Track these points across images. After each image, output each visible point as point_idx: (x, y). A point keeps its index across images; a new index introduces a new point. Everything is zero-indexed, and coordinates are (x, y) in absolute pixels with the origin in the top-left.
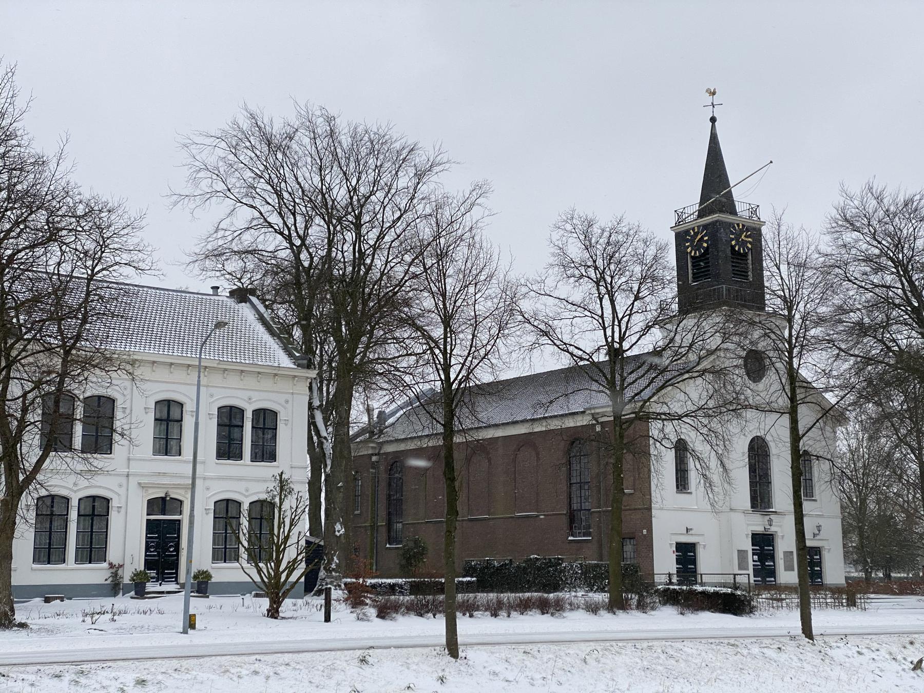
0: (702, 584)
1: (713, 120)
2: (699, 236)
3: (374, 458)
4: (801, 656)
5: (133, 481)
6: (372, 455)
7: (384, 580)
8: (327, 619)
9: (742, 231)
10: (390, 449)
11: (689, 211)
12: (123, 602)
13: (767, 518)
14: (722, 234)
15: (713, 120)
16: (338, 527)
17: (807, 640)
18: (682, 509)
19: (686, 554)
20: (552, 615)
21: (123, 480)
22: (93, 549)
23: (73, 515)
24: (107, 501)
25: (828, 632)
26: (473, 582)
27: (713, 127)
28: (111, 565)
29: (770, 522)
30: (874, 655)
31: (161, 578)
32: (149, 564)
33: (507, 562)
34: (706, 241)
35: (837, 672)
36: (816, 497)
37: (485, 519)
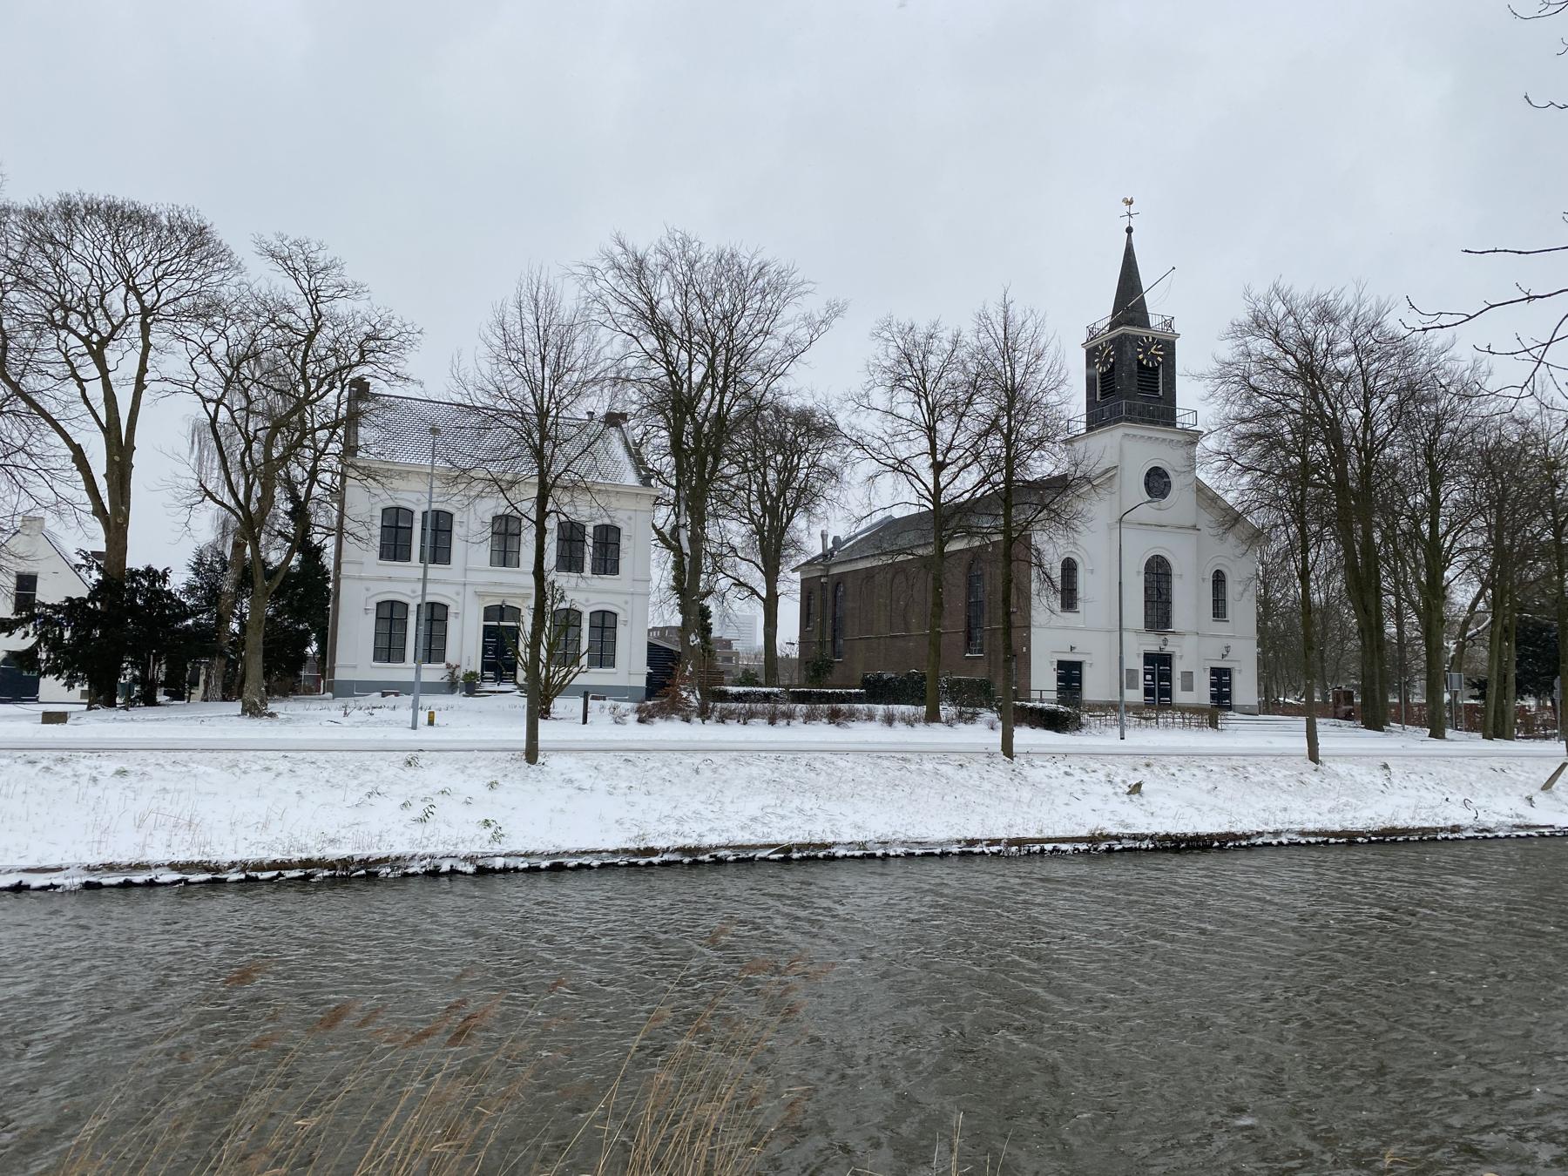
1: (1129, 230)
4: (985, 775)
5: (470, 589)
8: (585, 722)
9: (1152, 344)
10: (835, 571)
12: (457, 699)
15: (1129, 230)
16: (692, 637)
19: (1070, 674)
21: (461, 589)
22: (433, 649)
23: (585, 626)
24: (446, 607)
25: (1036, 750)
27: (1129, 237)
28: (449, 666)
29: (1165, 642)
30: (1085, 777)
31: (500, 678)
32: (486, 666)
35: (1026, 794)
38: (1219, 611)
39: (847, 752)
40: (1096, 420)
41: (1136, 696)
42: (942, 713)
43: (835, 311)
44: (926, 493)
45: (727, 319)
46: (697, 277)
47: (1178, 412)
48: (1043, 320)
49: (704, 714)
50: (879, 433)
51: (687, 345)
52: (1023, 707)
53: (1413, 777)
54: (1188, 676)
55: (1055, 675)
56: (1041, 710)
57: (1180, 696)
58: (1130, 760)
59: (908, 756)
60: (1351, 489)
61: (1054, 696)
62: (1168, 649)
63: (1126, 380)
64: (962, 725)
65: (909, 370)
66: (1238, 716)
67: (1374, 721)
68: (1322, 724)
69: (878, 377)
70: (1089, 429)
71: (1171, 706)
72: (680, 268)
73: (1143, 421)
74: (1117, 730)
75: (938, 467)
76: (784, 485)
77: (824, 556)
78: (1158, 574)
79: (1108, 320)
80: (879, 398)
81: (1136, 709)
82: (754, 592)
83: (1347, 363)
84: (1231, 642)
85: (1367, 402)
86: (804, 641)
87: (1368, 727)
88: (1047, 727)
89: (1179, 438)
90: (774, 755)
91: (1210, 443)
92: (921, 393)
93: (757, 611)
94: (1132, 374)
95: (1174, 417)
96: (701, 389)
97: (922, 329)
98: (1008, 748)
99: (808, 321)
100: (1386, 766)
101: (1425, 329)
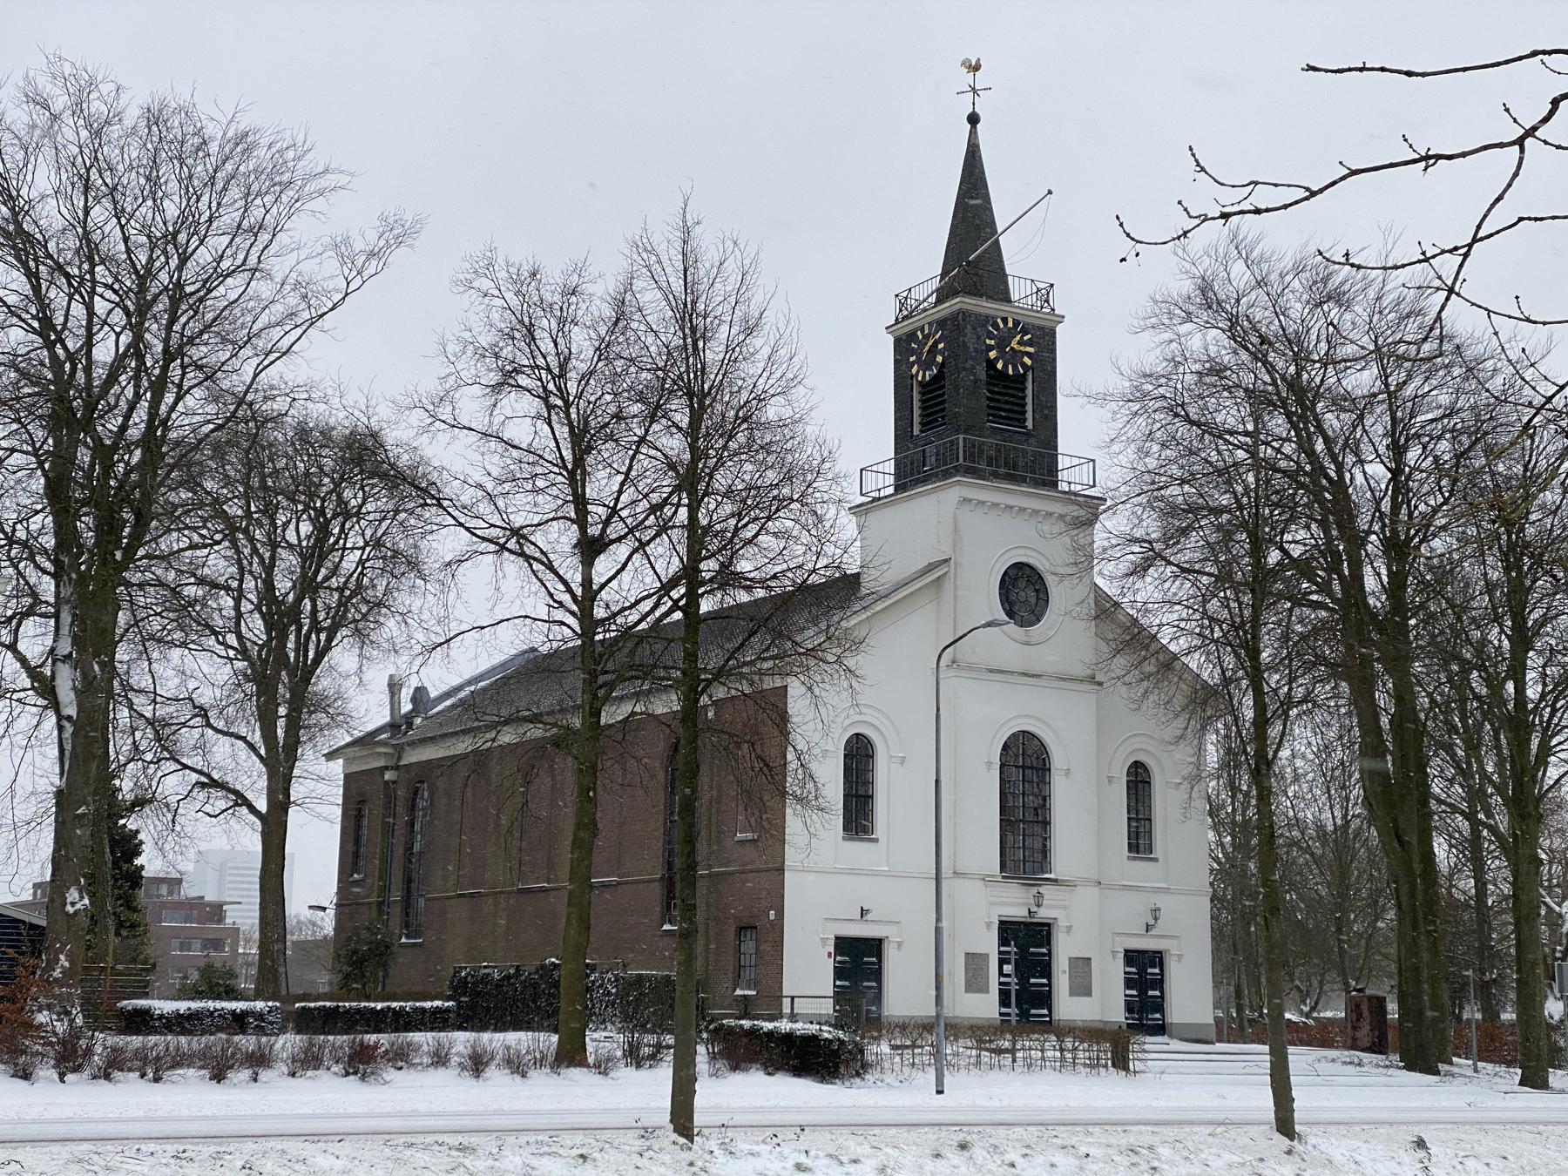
0: (793, 1017)
1: (973, 119)
2: (931, 342)
3: (387, 776)
6: (386, 768)
7: (219, 1005)
10: (413, 757)
11: (919, 294)
13: (1034, 890)
14: (970, 339)
15: (973, 119)
16: (73, 895)
17: (675, 1136)
18: (852, 872)
19: (859, 960)
20: (363, 1078)
25: (740, 1119)
26: (448, 1010)
27: (973, 133)
33: (512, 971)
34: (942, 352)
36: (1158, 851)
37: (543, 890)
38: (1140, 841)
39: (341, 1137)
40: (913, 471)
41: (986, 1006)
42: (590, 1048)
43: (397, 234)
44: (566, 598)
45: (170, 243)
46: (110, 152)
47: (1062, 462)
48: (755, 261)
49: (69, 1059)
50: (477, 476)
51: (83, 289)
52: (753, 1033)
53: (1470, 1163)
54: (1082, 966)
55: (829, 965)
56: (789, 1037)
57: (1068, 1007)
58: (930, 1135)
59: (474, 1140)
60: (1373, 615)
61: (827, 1008)
62: (1044, 914)
63: (968, 400)
64: (631, 1072)
65: (524, 354)
66: (1176, 1045)
67: (1423, 1054)
68: (1298, 1058)
69: (468, 367)
70: (899, 488)
71: (1049, 1026)
72: (71, 133)
73: (996, 476)
74: (931, 1074)
75: (590, 548)
76: (307, 586)
77: (393, 727)
78: (1025, 765)
79: (936, 284)
80: (471, 405)
81: (980, 1034)
82: (241, 800)
83: (1362, 380)
84: (1161, 901)
85: (1398, 451)
86: (346, 902)
87: (1410, 1067)
88: (798, 1071)
89: (1058, 508)
90: (172, 1148)
91: (1111, 526)
92: (555, 401)
93: (250, 840)
94: (975, 389)
95: (1053, 469)
96: (112, 378)
97: (554, 277)
98: (682, 1119)
99: (340, 248)
100: (1421, 1144)
101: (1225, 216)
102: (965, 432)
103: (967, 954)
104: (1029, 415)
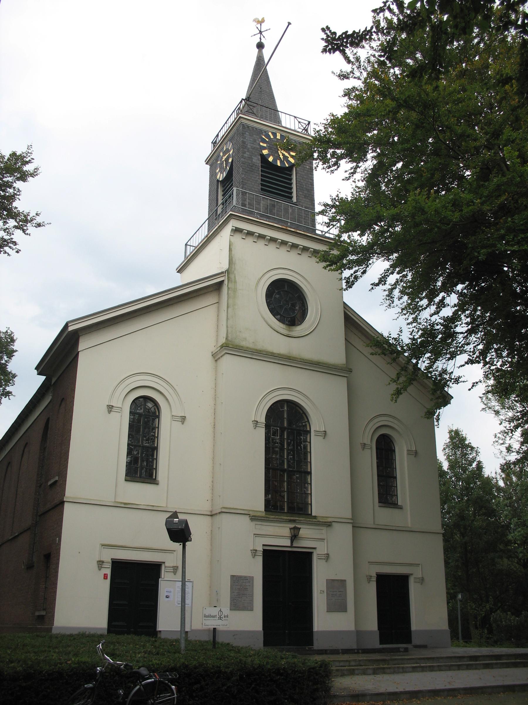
54: (336, 587)
62: (304, 544)
102: (237, 187)
103: (232, 577)
104: (294, 195)
